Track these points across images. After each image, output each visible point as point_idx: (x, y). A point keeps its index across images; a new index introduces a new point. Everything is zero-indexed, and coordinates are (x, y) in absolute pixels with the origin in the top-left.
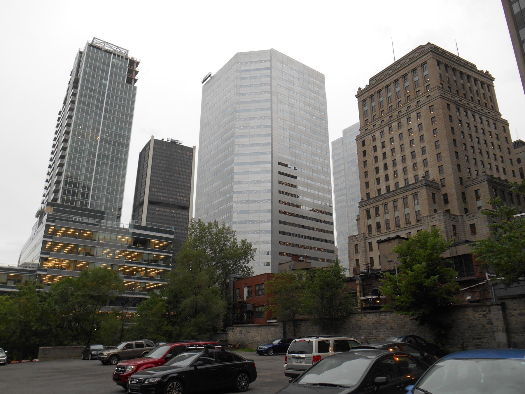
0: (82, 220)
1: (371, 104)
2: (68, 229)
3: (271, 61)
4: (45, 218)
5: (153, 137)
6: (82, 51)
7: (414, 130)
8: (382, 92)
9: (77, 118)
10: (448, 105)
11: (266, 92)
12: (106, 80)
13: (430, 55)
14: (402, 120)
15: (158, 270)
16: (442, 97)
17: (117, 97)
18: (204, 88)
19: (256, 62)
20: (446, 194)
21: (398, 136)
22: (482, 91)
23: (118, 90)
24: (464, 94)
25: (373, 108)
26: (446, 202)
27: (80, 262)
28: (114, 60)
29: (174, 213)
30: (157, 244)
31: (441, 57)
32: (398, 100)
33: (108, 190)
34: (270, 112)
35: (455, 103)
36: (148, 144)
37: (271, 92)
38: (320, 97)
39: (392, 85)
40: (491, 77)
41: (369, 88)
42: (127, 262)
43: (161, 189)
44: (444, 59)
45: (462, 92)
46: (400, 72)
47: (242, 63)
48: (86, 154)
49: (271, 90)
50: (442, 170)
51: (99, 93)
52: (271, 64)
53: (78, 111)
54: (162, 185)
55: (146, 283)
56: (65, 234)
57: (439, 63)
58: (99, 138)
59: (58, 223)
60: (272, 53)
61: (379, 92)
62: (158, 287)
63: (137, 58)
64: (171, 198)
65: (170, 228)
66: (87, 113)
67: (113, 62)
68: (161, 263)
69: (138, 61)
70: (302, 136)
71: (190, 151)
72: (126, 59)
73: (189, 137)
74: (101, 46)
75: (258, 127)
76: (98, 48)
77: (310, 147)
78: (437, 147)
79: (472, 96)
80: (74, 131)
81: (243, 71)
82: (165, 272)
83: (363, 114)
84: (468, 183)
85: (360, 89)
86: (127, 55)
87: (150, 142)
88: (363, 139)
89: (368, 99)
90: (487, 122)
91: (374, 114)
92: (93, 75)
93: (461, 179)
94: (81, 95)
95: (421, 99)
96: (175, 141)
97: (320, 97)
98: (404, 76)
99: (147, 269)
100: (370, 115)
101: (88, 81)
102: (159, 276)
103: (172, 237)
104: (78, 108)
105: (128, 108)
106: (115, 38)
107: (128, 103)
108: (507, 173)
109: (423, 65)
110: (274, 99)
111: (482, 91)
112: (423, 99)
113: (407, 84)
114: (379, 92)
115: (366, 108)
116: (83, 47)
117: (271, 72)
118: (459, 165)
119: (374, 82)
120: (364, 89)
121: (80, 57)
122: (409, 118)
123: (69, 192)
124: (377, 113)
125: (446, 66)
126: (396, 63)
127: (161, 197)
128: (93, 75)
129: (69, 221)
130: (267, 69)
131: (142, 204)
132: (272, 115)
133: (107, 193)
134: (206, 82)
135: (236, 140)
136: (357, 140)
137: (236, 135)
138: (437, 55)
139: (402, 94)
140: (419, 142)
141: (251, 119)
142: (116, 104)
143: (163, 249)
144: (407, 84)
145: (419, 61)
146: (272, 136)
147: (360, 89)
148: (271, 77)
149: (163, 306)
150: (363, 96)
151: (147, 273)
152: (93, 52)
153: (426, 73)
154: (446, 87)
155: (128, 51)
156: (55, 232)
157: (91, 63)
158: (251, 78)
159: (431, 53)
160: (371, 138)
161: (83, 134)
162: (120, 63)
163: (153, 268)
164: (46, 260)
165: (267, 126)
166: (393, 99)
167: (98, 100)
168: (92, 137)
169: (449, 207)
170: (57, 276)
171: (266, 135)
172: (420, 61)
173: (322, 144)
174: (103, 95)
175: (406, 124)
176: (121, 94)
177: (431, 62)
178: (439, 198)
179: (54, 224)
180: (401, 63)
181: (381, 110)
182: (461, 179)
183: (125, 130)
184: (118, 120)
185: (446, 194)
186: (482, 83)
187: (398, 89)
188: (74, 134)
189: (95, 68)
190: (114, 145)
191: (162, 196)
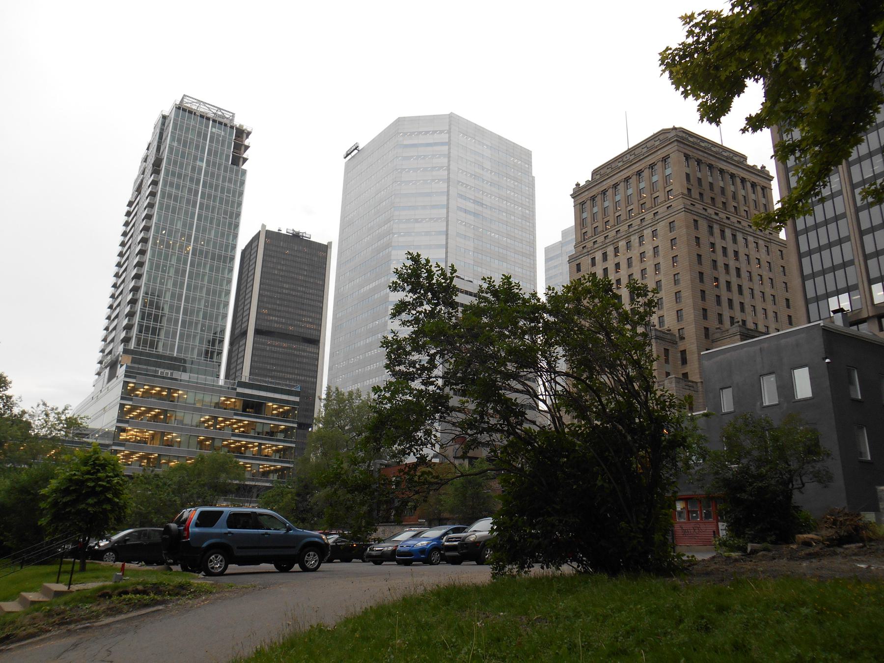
0: (172, 374)
1: (591, 210)
2: (153, 387)
3: (449, 132)
4: (121, 371)
5: (264, 226)
6: (167, 114)
7: (647, 255)
8: (607, 193)
9: (159, 219)
10: (696, 221)
11: (439, 180)
12: (202, 160)
13: (674, 147)
14: (632, 238)
15: (276, 446)
16: (687, 210)
17: (217, 186)
18: (347, 165)
19: (427, 133)
20: (685, 350)
21: (626, 261)
22: (752, 197)
23: (218, 176)
24: (724, 203)
25: (594, 216)
26: (684, 361)
27: (169, 434)
28: (214, 130)
29: (295, 349)
30: (275, 409)
31: (691, 149)
32: (629, 208)
33: (203, 325)
34: (445, 211)
35: (708, 219)
36: (257, 237)
37: (448, 180)
38: (523, 187)
39: (622, 184)
40: (769, 175)
41: (589, 185)
42: (234, 435)
43: (275, 310)
44: (695, 151)
45: (720, 200)
46: (634, 167)
47: (405, 134)
48: (172, 271)
49: (449, 178)
50: (682, 316)
51: (192, 180)
52: (449, 137)
53: (160, 208)
54: (276, 304)
55: (259, 465)
56: (146, 394)
57: (687, 157)
58: (191, 248)
59: (140, 379)
60: (452, 119)
61: (604, 192)
62: (276, 471)
63: (247, 126)
64: (292, 325)
65: (294, 386)
66: (174, 212)
67: (211, 132)
68: (281, 436)
69: (249, 130)
70: (492, 247)
71: (322, 250)
72: (232, 127)
73: (322, 226)
74: (194, 107)
75: (428, 233)
76: (190, 112)
77: (505, 264)
78: (676, 282)
79: (736, 205)
80: (155, 238)
81: (406, 146)
82: (285, 449)
83: (580, 222)
84: (717, 336)
85: (578, 185)
86: (232, 120)
87: (259, 234)
88: (578, 262)
89: (589, 202)
90: (754, 245)
91: (595, 225)
92: (183, 153)
93: (706, 329)
94: (165, 185)
95: (660, 211)
96: (299, 233)
97: (523, 187)
98: (639, 173)
99: (260, 444)
100: (589, 225)
101: (175, 162)
102: (278, 455)
103: (297, 399)
104: (161, 204)
105: (233, 202)
106: (214, 95)
107: (234, 196)
108: (779, 320)
109: (665, 159)
110: (453, 192)
111: (752, 197)
112: (662, 210)
113: (642, 185)
114: (604, 192)
115: (585, 215)
116: (167, 108)
117: (449, 149)
118: (705, 310)
119: (598, 177)
120: (584, 186)
121: (163, 124)
122: (641, 238)
123: (147, 328)
124: (600, 224)
125: (699, 162)
126: (630, 151)
127: (275, 323)
128: (183, 153)
129: (155, 376)
130: (442, 144)
131: (244, 334)
132: (448, 216)
133: (202, 330)
134: (350, 157)
135: (393, 252)
136: (570, 262)
137: (393, 244)
138: (686, 147)
139: (635, 199)
140: (653, 274)
141: (416, 221)
142: (215, 197)
143: (284, 416)
144: (642, 185)
145: (659, 152)
146: (447, 248)
147: (578, 185)
148: (449, 157)
149: (293, 499)
150: (583, 197)
151: (260, 450)
152: (183, 118)
153: (668, 172)
154: (695, 194)
155: (234, 114)
156: (134, 389)
157: (180, 135)
158: (418, 157)
159: (676, 143)
160: (590, 261)
161: (168, 243)
162: (223, 133)
163: (269, 443)
164: (124, 430)
165: (439, 233)
166: (623, 204)
167: (190, 190)
168: (181, 247)
169: (687, 369)
170: (136, 453)
171: (438, 246)
172: (661, 154)
173: (524, 259)
174: (198, 183)
175: (638, 245)
176: (224, 181)
177: (676, 158)
178: (674, 355)
179: (134, 381)
180: (637, 152)
181: (606, 220)
182: (706, 329)
183: (228, 235)
184: (218, 220)
185: (685, 350)
186: (754, 185)
187: (630, 192)
188: (155, 243)
189: (185, 142)
190: (213, 259)
191: (277, 322)
